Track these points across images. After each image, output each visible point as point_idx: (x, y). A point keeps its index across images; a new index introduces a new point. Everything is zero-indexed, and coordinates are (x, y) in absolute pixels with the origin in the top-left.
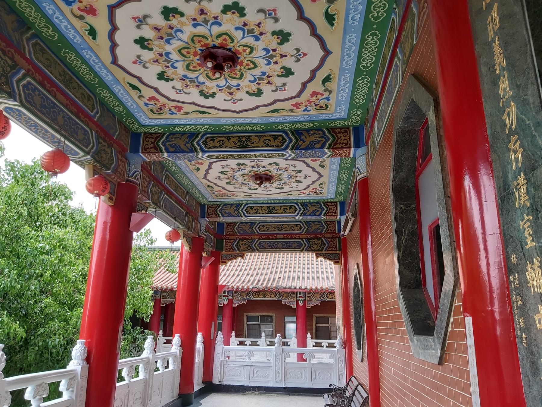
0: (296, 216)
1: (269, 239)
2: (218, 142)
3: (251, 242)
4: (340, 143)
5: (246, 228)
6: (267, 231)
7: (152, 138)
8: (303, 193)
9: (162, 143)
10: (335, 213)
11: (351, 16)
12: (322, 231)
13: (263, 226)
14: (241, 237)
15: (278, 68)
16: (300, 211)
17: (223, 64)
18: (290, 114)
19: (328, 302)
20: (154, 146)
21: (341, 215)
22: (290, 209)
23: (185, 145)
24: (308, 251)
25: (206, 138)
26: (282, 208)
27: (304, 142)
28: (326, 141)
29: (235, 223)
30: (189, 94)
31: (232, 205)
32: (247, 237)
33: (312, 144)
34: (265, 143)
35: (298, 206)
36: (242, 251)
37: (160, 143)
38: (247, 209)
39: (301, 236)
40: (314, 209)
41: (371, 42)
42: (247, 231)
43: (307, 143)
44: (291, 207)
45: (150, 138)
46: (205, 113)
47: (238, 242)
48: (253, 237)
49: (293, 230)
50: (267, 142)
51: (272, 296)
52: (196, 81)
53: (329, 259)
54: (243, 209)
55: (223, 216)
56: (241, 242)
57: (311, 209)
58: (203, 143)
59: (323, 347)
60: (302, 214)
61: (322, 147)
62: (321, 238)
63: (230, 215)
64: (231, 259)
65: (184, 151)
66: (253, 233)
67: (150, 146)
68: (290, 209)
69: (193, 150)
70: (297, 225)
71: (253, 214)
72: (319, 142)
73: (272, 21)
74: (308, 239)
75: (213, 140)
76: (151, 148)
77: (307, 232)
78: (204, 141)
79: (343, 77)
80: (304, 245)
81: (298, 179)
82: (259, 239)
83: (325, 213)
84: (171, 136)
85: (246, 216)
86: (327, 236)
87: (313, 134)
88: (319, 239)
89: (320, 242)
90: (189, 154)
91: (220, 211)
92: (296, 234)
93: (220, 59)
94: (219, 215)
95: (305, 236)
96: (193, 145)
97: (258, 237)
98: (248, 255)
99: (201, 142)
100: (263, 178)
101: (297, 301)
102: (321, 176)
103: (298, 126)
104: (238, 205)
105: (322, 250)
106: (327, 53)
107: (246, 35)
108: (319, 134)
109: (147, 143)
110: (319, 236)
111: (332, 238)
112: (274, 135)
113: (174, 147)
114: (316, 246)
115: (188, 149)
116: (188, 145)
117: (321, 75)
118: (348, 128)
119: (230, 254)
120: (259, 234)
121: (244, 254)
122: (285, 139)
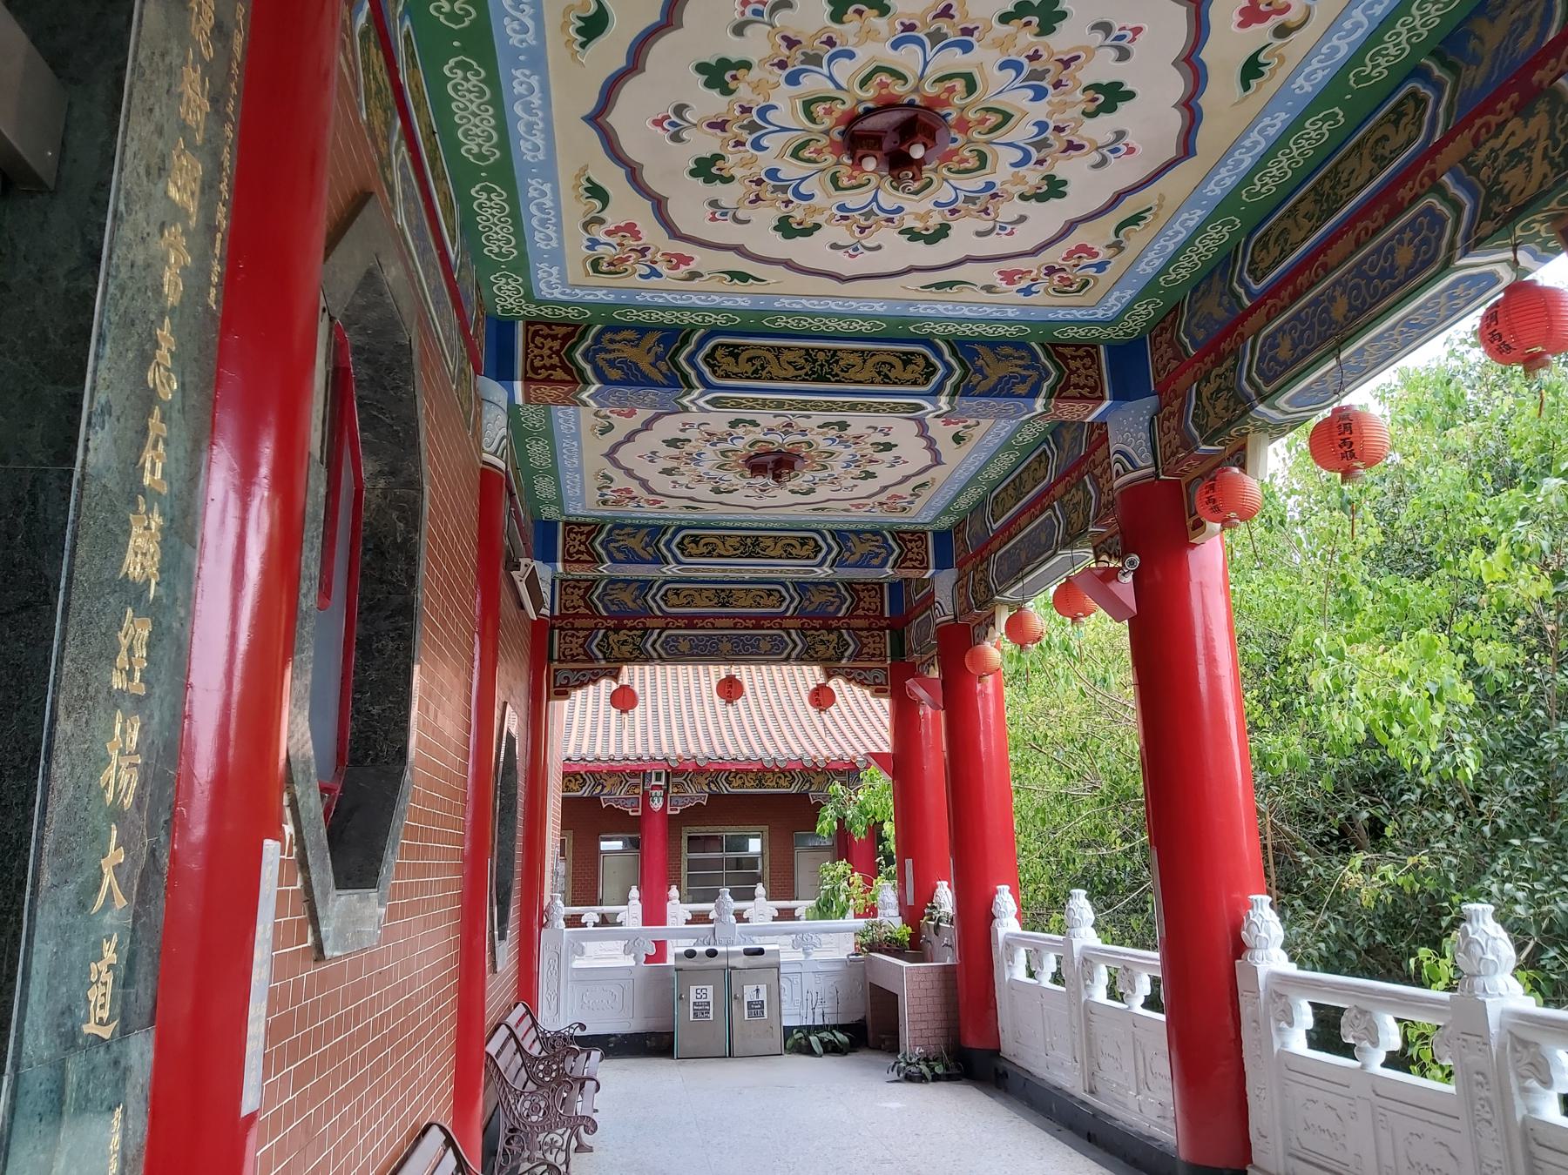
0: (820, 565)
1: (694, 628)
2: (749, 360)
3: (642, 637)
4: (1076, 386)
5: (627, 597)
6: (688, 605)
7: (554, 338)
8: (857, 506)
9: (585, 355)
10: (922, 562)
11: (1307, 70)
12: (839, 609)
13: (677, 592)
14: (611, 623)
15: (744, 93)
16: (828, 553)
17: (903, 148)
18: (985, 296)
19: (731, 795)
20: (561, 360)
21: (940, 566)
22: (802, 545)
23: (653, 365)
24: (800, 660)
25: (715, 348)
26: (876, 359)
27: (985, 377)
28: (1042, 379)
29: (646, 582)
30: (879, 247)
31: (639, 527)
32: (629, 623)
33: (1007, 383)
34: (879, 373)
35: (825, 539)
36: (617, 660)
37: (578, 356)
38: (681, 542)
39: (786, 623)
40: (867, 547)
41: (1313, 134)
42: (630, 604)
43: (994, 379)
44: (803, 542)
45: (545, 337)
46: (743, 277)
47: (605, 636)
48: (649, 623)
49: (758, 605)
50: (885, 369)
51: (571, 785)
52: (876, 210)
53: (862, 683)
54: (828, 553)
55: (613, 560)
56: (613, 637)
57: (861, 549)
58: (705, 360)
59: (585, 925)
60: (834, 561)
61: (1033, 393)
62: (838, 629)
63: (633, 558)
64: (582, 685)
65: (653, 384)
66: (647, 613)
67: (547, 362)
68: (802, 545)
69: (679, 382)
70: (770, 593)
71: (737, 376)
72: (1024, 379)
73: (1114, 54)
74: (802, 630)
75: (736, 356)
76: (553, 367)
77: (800, 613)
78: (707, 356)
79: (1186, 216)
80: (791, 645)
81: (676, 452)
82: (663, 630)
83: (896, 562)
84: (608, 336)
85: (679, 563)
86: (590, 623)
87: (1007, 357)
88: (830, 630)
89: (834, 637)
90: (660, 392)
91: (603, 544)
92: (772, 617)
93: (894, 137)
94: (581, 372)
95: (798, 623)
96: (677, 366)
97: (662, 623)
98: (191, 680)
99: (699, 359)
100: (774, 464)
101: (646, 796)
102: (937, 461)
103: (966, 330)
104: (656, 530)
105: (839, 660)
106: (1187, 148)
107: (930, 54)
108: (1022, 358)
109: (537, 351)
110: (834, 623)
111: (868, 629)
112: (904, 353)
113: (621, 369)
114: (822, 648)
115: (665, 376)
116: (663, 366)
117: (610, 51)
118: (1095, 347)
119: (579, 670)
120: (666, 615)
121: (619, 669)
122: (933, 365)
